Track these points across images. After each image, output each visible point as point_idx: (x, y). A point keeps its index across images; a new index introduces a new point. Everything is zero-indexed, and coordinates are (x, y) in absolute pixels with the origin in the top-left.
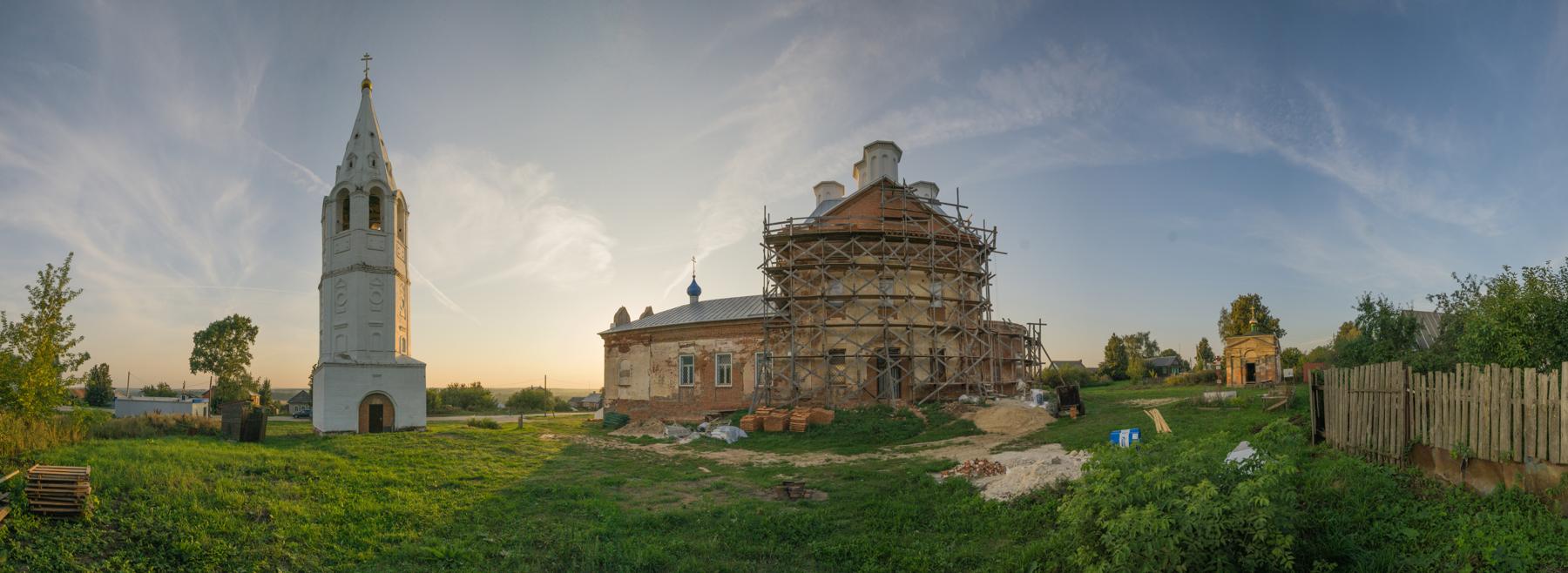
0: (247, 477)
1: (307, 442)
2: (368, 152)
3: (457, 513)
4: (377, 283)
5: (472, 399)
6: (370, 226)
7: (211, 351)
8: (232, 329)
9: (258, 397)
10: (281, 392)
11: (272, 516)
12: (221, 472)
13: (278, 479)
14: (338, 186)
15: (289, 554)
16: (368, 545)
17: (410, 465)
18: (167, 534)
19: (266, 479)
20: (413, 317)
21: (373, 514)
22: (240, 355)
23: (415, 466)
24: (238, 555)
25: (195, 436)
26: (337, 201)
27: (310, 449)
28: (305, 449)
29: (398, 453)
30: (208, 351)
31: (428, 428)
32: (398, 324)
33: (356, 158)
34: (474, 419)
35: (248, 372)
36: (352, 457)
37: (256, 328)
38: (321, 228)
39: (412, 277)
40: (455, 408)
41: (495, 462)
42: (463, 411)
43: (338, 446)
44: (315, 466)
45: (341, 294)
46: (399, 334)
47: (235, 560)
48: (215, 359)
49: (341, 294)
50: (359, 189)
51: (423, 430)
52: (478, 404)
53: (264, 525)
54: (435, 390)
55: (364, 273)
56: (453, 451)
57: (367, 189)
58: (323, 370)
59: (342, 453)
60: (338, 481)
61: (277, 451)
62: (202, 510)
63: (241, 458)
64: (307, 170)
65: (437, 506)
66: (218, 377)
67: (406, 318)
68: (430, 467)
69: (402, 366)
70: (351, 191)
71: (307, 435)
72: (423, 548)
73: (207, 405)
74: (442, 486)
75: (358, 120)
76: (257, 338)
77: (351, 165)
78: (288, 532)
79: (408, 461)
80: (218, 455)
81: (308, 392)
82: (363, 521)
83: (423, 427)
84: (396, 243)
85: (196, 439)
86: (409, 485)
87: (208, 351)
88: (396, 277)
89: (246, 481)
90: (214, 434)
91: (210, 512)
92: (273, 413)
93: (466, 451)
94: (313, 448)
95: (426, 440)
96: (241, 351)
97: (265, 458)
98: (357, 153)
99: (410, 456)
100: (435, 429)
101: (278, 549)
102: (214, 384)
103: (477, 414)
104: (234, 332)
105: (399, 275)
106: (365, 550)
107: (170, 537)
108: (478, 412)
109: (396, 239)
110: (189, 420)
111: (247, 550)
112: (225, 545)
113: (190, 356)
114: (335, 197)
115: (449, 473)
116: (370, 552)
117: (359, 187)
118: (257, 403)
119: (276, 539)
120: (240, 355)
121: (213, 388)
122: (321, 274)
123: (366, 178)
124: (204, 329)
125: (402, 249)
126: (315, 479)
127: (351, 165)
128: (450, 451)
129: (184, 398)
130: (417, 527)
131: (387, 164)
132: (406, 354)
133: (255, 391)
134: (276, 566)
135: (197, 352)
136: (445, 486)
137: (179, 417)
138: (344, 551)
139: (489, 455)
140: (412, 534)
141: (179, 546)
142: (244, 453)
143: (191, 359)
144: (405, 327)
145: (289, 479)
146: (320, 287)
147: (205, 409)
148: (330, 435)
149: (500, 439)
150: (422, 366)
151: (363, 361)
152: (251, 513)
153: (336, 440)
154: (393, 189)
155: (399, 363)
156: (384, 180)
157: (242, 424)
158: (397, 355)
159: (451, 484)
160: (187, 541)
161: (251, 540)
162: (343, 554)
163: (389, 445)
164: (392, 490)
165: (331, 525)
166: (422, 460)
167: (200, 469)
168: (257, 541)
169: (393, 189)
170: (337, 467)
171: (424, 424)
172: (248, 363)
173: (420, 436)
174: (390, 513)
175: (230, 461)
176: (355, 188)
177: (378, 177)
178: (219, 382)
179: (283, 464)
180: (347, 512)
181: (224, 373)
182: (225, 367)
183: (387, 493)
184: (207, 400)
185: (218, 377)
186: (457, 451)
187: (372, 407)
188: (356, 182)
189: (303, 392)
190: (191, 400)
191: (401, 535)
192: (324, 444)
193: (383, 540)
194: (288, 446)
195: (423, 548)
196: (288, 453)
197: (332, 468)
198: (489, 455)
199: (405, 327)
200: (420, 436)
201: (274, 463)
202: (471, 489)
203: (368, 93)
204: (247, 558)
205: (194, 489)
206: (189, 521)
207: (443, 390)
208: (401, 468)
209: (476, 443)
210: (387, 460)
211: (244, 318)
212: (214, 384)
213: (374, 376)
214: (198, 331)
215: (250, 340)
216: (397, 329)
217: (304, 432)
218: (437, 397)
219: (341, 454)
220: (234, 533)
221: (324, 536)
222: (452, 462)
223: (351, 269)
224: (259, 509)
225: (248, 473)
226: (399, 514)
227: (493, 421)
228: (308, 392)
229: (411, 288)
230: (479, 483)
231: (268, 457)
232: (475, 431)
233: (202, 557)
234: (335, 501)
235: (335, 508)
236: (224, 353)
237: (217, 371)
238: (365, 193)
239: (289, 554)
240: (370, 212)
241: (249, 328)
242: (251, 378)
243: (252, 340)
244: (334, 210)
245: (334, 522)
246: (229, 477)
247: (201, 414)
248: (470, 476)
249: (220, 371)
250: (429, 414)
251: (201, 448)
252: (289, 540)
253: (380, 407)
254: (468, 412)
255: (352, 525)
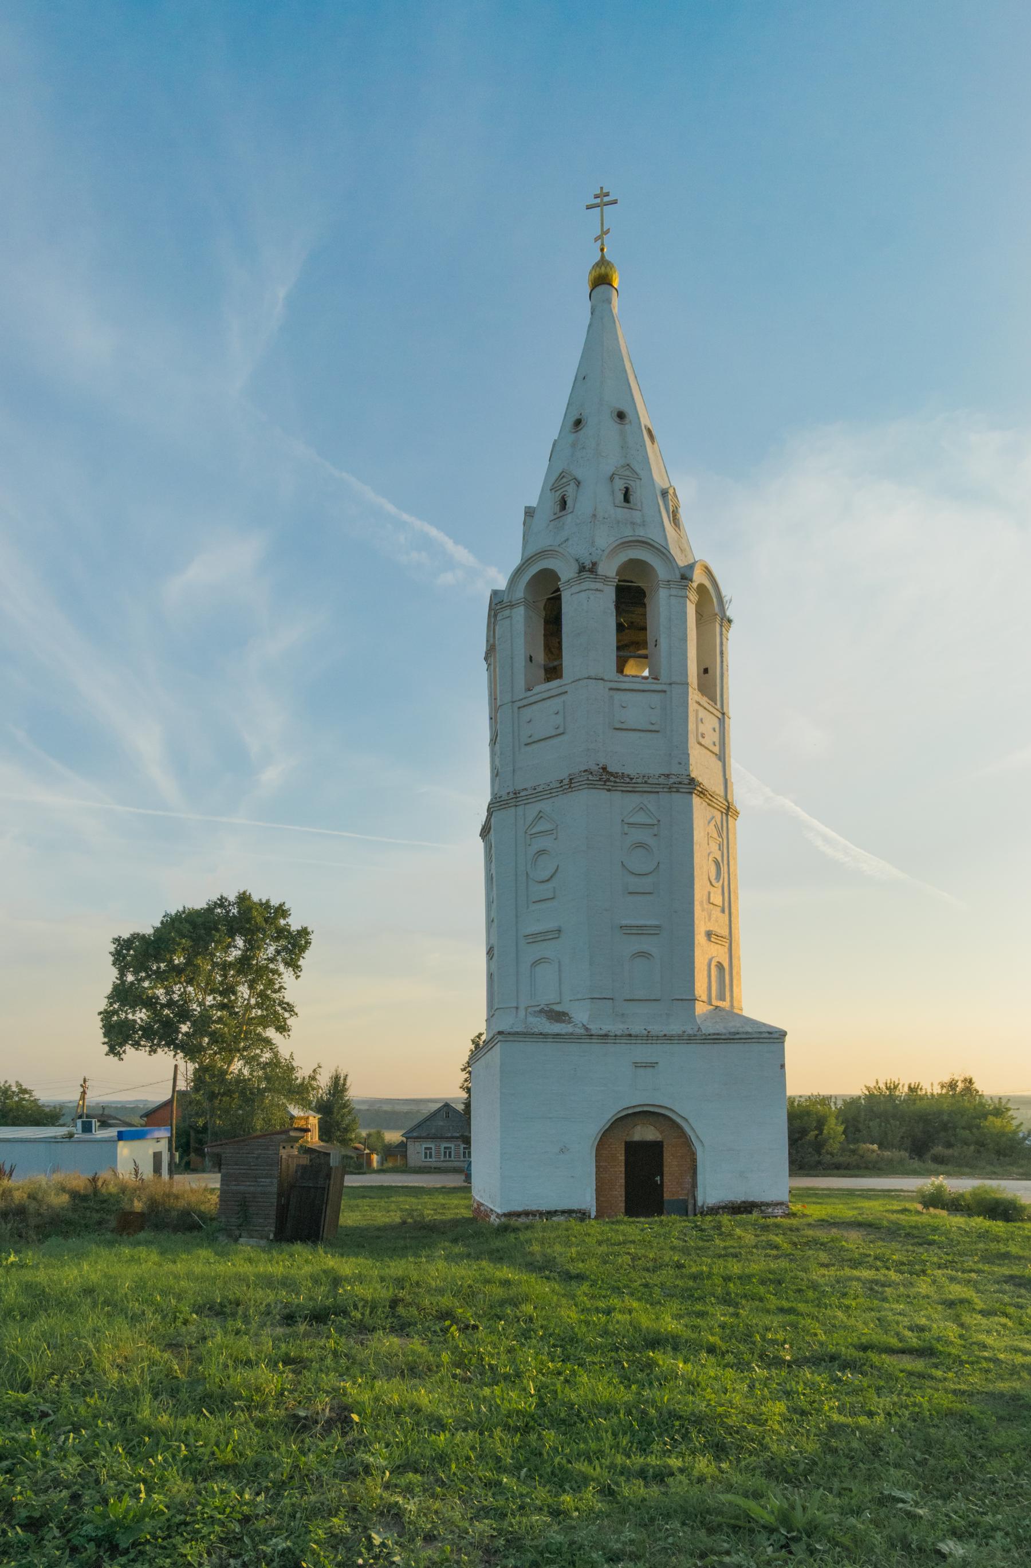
0: (288, 1330)
1: (455, 1241)
2: (611, 463)
3: (834, 1430)
4: (641, 818)
5: (945, 1127)
6: (620, 670)
7: (169, 992)
8: (231, 933)
9: (314, 1120)
10: (387, 1108)
11: (355, 1417)
12: (215, 1322)
13: (374, 1330)
14: (527, 562)
15: (400, 1500)
16: (586, 1479)
17: (726, 1300)
18: (65, 1493)
19: (340, 1331)
20: (745, 901)
21: (608, 1412)
22: (258, 1005)
23: (736, 1305)
24: (269, 1513)
25: (142, 1235)
26: (527, 603)
27: (461, 1257)
28: (447, 1258)
29: (694, 1270)
30: (160, 992)
31: (796, 1208)
32: (701, 927)
33: (578, 483)
34: (939, 1189)
35: (284, 1052)
36: (569, 1277)
37: (304, 932)
38: (485, 676)
39: (739, 796)
40: (887, 1154)
41: (984, 1313)
42: (916, 1164)
43: (536, 1248)
44: (468, 1296)
45: (541, 852)
46: (705, 952)
47: (260, 1525)
48: (184, 1014)
49: (541, 852)
50: (588, 570)
51: (779, 1211)
52: (966, 1143)
53: (337, 1441)
54: (825, 1100)
55: (604, 795)
56: (856, 1273)
57: (609, 568)
58: (495, 1055)
59: (544, 1267)
60: (526, 1334)
61: (370, 1262)
62: (164, 1419)
63: (268, 1282)
64: (434, 532)
65: (780, 1407)
66: (192, 1067)
67: (728, 908)
68: (782, 1310)
69: (715, 1039)
70: (564, 579)
71: (456, 1223)
72: (724, 1498)
73: (163, 1146)
74: (807, 1361)
75: (581, 378)
76: (306, 961)
77: (563, 504)
78: (397, 1452)
79: (719, 1291)
80: (202, 1278)
81: (460, 1107)
82: (581, 1426)
83: (781, 1204)
84: (692, 706)
85: (148, 1243)
86: (711, 1350)
87: (160, 992)
88: (696, 800)
89: (286, 1338)
90: (194, 1227)
91: (190, 1421)
92: (361, 1166)
93: (893, 1275)
94: (468, 1256)
95: (778, 1240)
96: (262, 995)
97: (336, 1281)
98: (579, 473)
99: (727, 1279)
100: (816, 1211)
101: (374, 1489)
102: (182, 1086)
103: (948, 1174)
104: (240, 942)
105: (703, 793)
106: (577, 1490)
107: (75, 1498)
108: (944, 1164)
109: (694, 695)
110: (113, 1189)
111: (289, 1498)
112: (234, 1494)
113: (103, 1004)
114: (520, 593)
115: (832, 1329)
116: (589, 1493)
117: (588, 564)
118: (313, 1139)
119: (367, 1469)
120: (258, 1005)
121: (180, 1096)
122: (487, 798)
123: (604, 539)
124: (148, 931)
125: (710, 723)
126: (466, 1328)
127: (563, 504)
128: (848, 1272)
129: (87, 1128)
130: (719, 1450)
131: (664, 493)
132: (725, 1005)
133: (305, 1104)
134: (366, 1529)
135: (122, 994)
136: (816, 1361)
137: (79, 1181)
138: (524, 1490)
139: (968, 1293)
140: (703, 1465)
141: (104, 1516)
142: (277, 1269)
143: (106, 1016)
144: (725, 932)
145: (402, 1328)
146: (485, 832)
147: (157, 1156)
148: (514, 1222)
149: (1014, 1249)
150: (776, 1037)
151: (606, 1028)
152: (302, 1413)
153: (529, 1234)
154: (681, 562)
155: (709, 1028)
156: (658, 539)
157: (280, 1195)
158: (701, 1009)
159: (833, 1358)
160: (126, 1498)
161: (301, 1479)
162: (522, 1495)
163: (673, 1248)
164: (663, 1360)
165: (498, 1432)
166: (762, 1289)
167: (153, 1320)
168: (319, 1477)
169: (681, 562)
170: (526, 1299)
171: (785, 1197)
172: (282, 1029)
173: (765, 1228)
174: (652, 1412)
175: (237, 1291)
176: (575, 567)
177: (641, 533)
178: (198, 1080)
179: (385, 1294)
180: (541, 1404)
181: (211, 1055)
182: (216, 1038)
183: (651, 1364)
184: (163, 1133)
185: (192, 1067)
186: (866, 1274)
187: (633, 1149)
188: (578, 549)
189: (447, 1108)
190: (112, 1132)
191: (674, 1462)
192: (497, 1243)
193: (624, 1471)
194: (398, 1252)
195: (724, 1498)
196: (397, 1268)
197: (515, 1302)
198: (968, 1293)
199: (725, 932)
200: (765, 1228)
201: (360, 1290)
202: (890, 1377)
203: (609, 301)
204: (293, 1516)
205: (136, 1373)
206: (129, 1453)
207: (852, 1103)
208: (698, 1307)
209: (932, 1255)
210: (662, 1285)
211: (267, 905)
212: (182, 1086)
213: (637, 1065)
214: (126, 935)
215: (287, 964)
216: (700, 938)
217: (449, 1215)
218: (832, 1121)
219: (541, 1269)
220: (257, 1465)
221: (480, 1457)
222: (847, 1302)
223: (570, 784)
224: (323, 1405)
225: (289, 1319)
226: (674, 1415)
227: (1008, 1195)
228: (460, 1107)
229: (741, 828)
230: (919, 1365)
231: (347, 1279)
232: (936, 1222)
233: (172, 1529)
234: (514, 1379)
235: (513, 1395)
236: (209, 1000)
237: (191, 1050)
238: (606, 579)
239: (400, 1500)
240: (620, 627)
241: (282, 933)
242: (291, 1069)
243: (293, 964)
244: (522, 612)
245: (507, 1427)
246: (238, 1332)
247: (147, 1171)
248: (894, 1342)
249: (200, 1049)
250: (799, 1166)
251: (168, 1267)
252: (399, 1470)
253: (655, 1149)
254: (933, 1166)
255: (551, 1436)
